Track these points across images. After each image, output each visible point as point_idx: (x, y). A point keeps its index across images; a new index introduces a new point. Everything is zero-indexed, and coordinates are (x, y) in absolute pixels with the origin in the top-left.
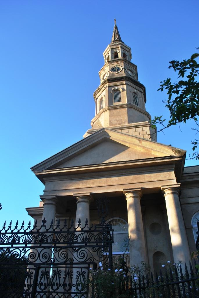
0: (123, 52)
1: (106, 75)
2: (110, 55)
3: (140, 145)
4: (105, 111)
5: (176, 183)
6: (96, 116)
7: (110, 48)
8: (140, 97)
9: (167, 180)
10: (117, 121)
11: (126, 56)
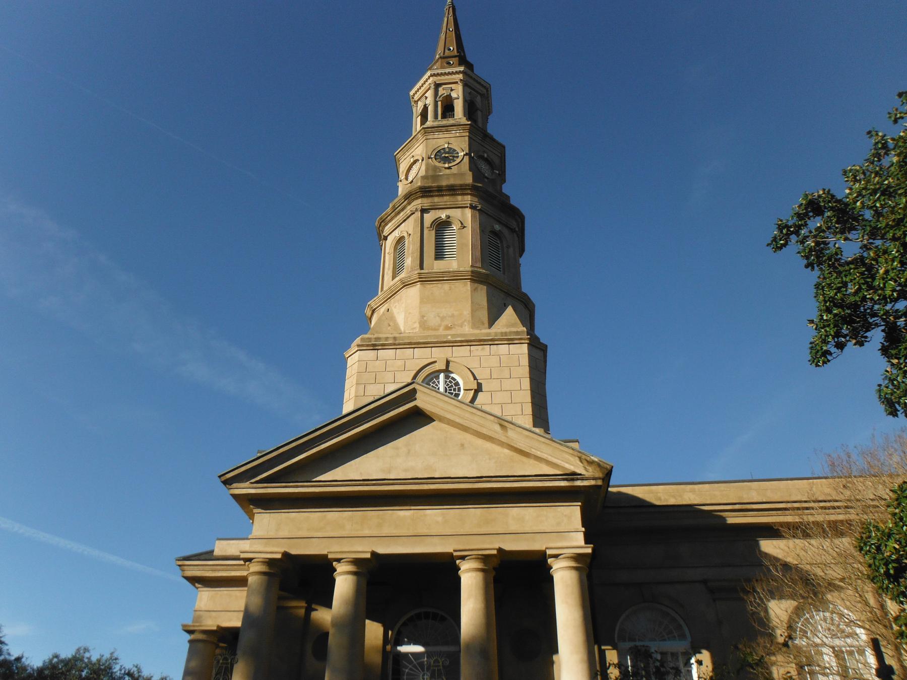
0: (468, 98)
1: (415, 168)
2: (430, 101)
3: (503, 439)
4: (406, 285)
5: (581, 542)
6: (380, 293)
7: (430, 81)
8: (508, 247)
9: (560, 533)
10: (443, 319)
11: (477, 109)
